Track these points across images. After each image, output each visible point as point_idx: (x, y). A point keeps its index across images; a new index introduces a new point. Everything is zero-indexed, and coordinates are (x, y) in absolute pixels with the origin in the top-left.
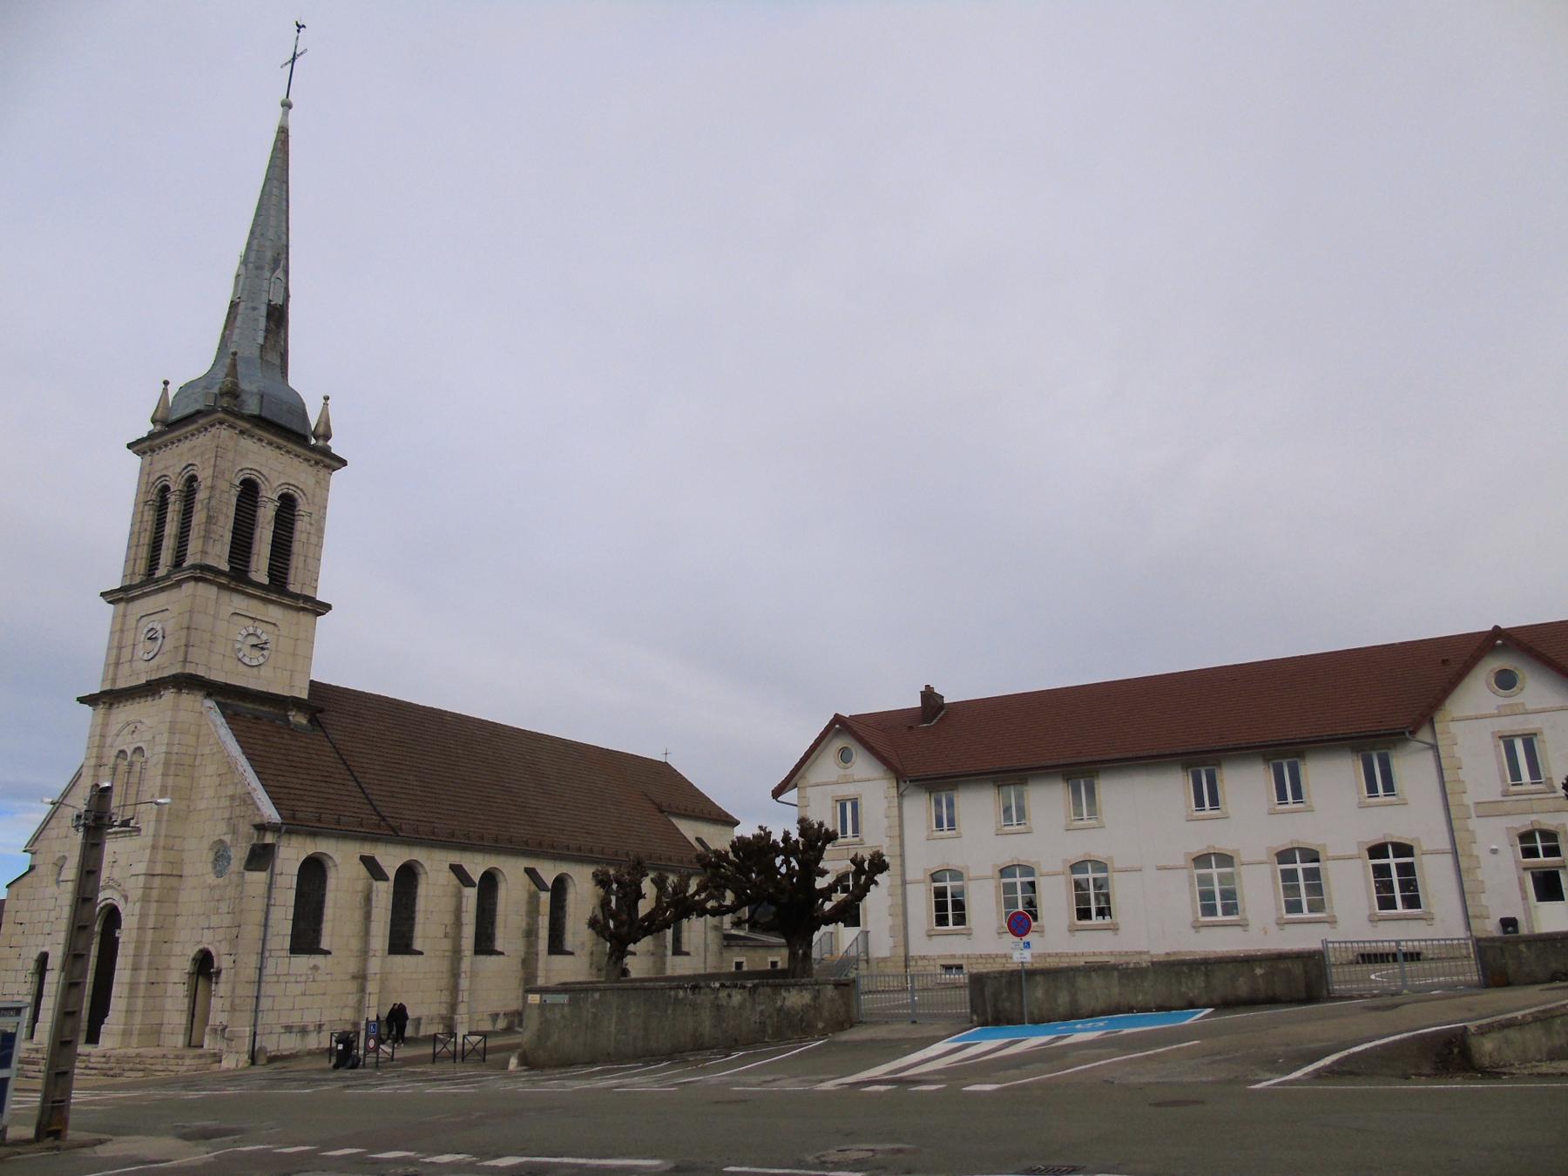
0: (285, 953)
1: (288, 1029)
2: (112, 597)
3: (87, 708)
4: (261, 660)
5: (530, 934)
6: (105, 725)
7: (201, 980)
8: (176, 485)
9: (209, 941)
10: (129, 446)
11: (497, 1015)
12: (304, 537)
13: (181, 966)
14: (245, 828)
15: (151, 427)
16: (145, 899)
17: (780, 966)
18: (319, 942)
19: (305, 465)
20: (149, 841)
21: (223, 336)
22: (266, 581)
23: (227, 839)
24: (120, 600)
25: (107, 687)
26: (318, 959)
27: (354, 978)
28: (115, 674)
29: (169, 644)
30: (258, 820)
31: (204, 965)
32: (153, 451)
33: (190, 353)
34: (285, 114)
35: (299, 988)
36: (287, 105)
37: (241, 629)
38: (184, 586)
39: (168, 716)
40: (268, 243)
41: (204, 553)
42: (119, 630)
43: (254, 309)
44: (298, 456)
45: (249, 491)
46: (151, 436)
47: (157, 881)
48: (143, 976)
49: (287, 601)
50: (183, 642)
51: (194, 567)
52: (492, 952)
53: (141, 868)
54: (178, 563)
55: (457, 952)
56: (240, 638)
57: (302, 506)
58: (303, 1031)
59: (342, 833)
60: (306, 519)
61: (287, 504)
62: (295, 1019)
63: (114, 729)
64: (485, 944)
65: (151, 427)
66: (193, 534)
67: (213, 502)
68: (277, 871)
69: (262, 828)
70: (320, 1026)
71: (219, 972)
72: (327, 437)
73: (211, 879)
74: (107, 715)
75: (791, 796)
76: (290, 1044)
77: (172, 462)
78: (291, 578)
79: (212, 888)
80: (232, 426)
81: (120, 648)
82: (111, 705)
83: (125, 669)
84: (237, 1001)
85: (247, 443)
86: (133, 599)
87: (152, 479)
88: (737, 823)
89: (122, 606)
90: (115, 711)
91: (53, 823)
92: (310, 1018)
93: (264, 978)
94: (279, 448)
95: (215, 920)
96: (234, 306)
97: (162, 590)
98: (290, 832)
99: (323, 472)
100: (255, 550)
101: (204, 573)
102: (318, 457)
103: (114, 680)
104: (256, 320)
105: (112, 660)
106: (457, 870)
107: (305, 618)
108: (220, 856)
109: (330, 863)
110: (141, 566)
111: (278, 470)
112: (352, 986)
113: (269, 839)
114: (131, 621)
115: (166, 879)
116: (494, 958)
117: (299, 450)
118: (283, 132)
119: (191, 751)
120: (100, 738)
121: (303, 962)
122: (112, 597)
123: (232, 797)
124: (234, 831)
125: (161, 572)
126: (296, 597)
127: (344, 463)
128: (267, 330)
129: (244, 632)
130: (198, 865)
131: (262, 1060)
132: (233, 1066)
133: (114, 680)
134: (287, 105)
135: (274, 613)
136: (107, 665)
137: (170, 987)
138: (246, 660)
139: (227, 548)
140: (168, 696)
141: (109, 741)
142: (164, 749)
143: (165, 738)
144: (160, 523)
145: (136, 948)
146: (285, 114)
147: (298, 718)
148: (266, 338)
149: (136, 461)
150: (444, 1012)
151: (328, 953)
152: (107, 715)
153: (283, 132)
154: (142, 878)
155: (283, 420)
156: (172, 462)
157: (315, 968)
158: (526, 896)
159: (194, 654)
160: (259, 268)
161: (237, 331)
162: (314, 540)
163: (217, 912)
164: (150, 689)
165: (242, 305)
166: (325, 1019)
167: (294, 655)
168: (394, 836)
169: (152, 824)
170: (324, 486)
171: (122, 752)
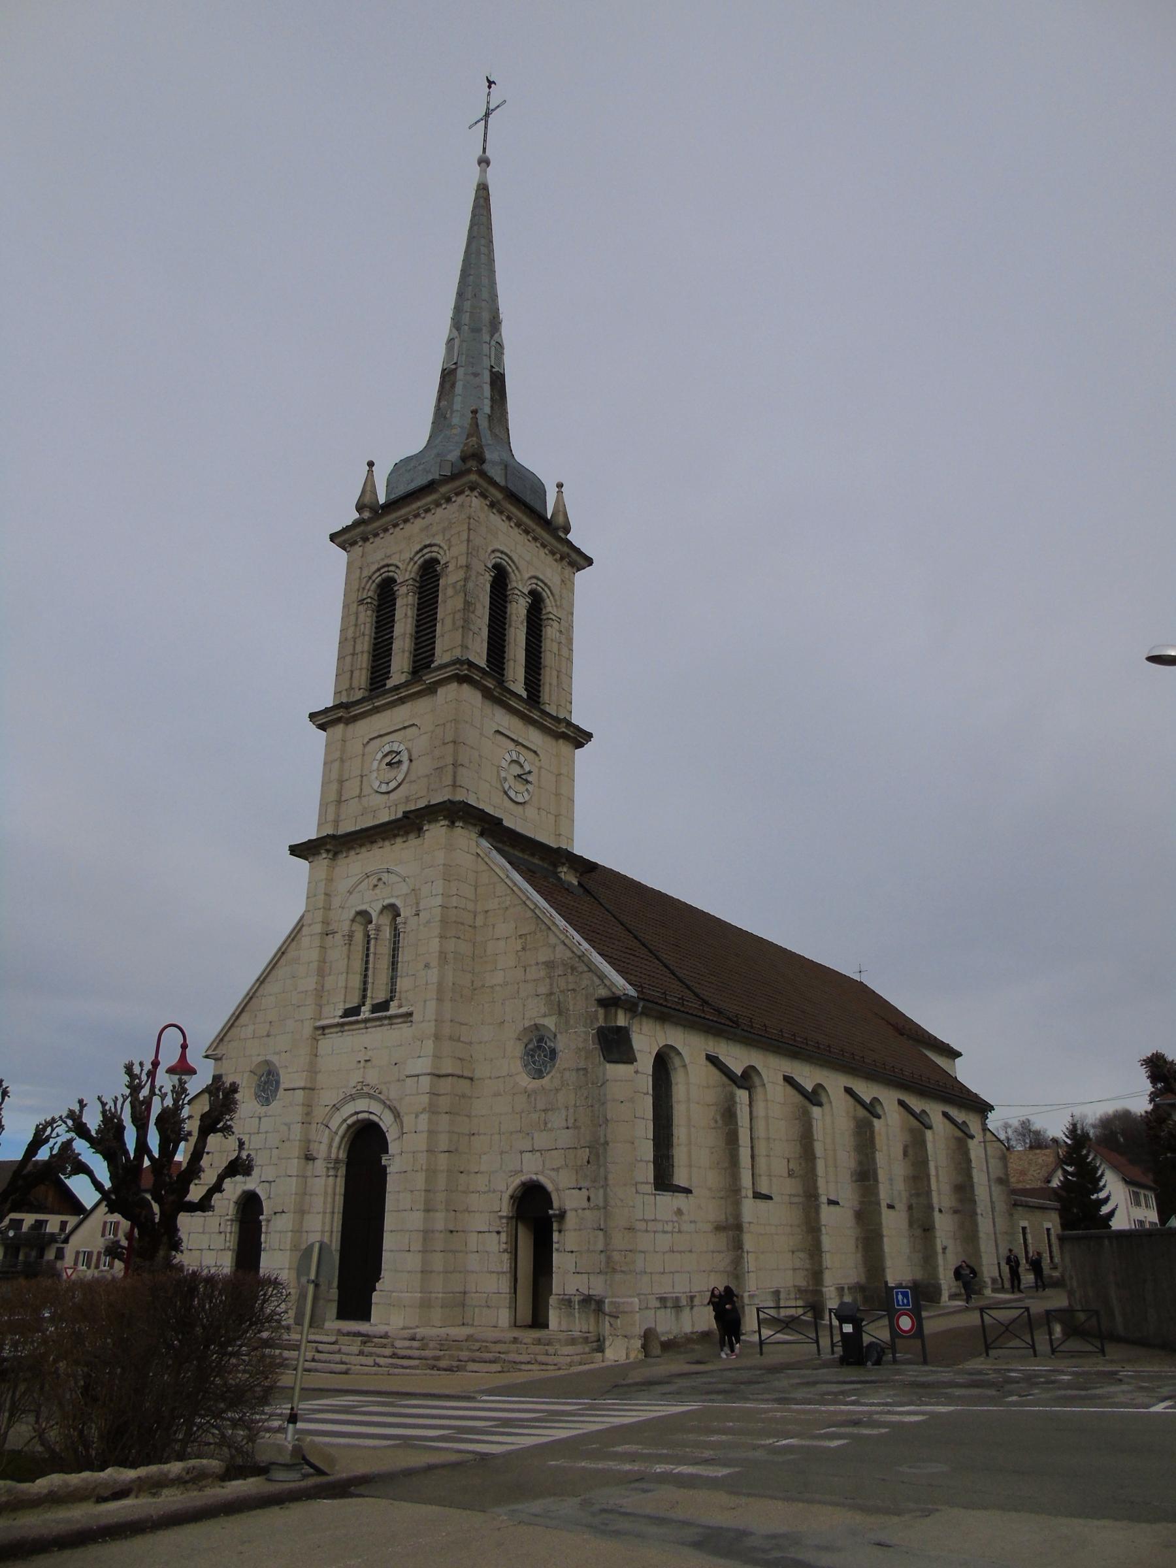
0: (650, 1188)
2: (323, 720)
3: (303, 864)
4: (527, 797)
6: (330, 880)
8: (406, 574)
9: (532, 1169)
10: (333, 537)
11: (843, 1288)
12: (555, 647)
13: (490, 1203)
14: (579, 1005)
15: (357, 515)
16: (432, 1110)
18: (671, 1175)
19: (550, 559)
20: (430, 1028)
21: (438, 408)
23: (550, 1022)
24: (338, 720)
25: (329, 830)
27: (719, 1228)
28: (338, 815)
29: (423, 766)
30: (603, 992)
31: (533, 1211)
32: (365, 539)
33: (401, 427)
34: (483, 172)
35: (664, 1241)
37: (505, 753)
38: (441, 691)
39: (440, 857)
40: (484, 304)
41: (464, 647)
42: (336, 762)
44: (544, 546)
46: (356, 524)
47: (445, 1085)
48: (440, 1220)
50: (450, 760)
53: (423, 1065)
56: (504, 764)
57: (550, 606)
60: (555, 624)
61: (536, 602)
62: (664, 1287)
63: (343, 886)
65: (357, 515)
66: (485, 599)
67: (470, 585)
69: (610, 1003)
70: (692, 1298)
71: (562, 1216)
72: (567, 530)
73: (525, 1081)
74: (331, 868)
77: (400, 550)
79: (528, 1094)
80: (483, 495)
81: (341, 782)
82: (336, 854)
83: (352, 808)
84: (616, 1256)
85: (495, 519)
86: (355, 719)
87: (366, 573)
89: (339, 729)
90: (342, 861)
91: (244, 1018)
92: (680, 1287)
94: (527, 532)
95: (541, 1140)
96: (448, 377)
97: (402, 701)
98: (646, 1014)
99: (568, 570)
101: (464, 673)
103: (336, 822)
104: (480, 387)
105: (333, 796)
107: (564, 747)
108: (539, 1051)
109: (677, 1062)
110: (362, 678)
112: (721, 1241)
113: (621, 1020)
114: (355, 747)
115: (455, 1082)
118: (483, 192)
119: (470, 906)
120: (321, 898)
122: (323, 720)
123: (550, 965)
124: (560, 1011)
127: (589, 561)
128: (492, 399)
129: (509, 759)
130: (503, 1062)
131: (656, 1350)
132: (622, 1359)
133: (336, 822)
134: (484, 162)
135: (534, 737)
136: (324, 805)
137: (473, 1239)
138: (512, 794)
139: (485, 645)
140: (436, 832)
141: (336, 902)
142: (439, 901)
143: (439, 887)
145: (428, 1180)
146: (483, 172)
148: (492, 407)
149: (339, 557)
150: (802, 1283)
151: (688, 1191)
152: (331, 868)
153: (483, 192)
154: (425, 1081)
155: (529, 498)
156: (400, 550)
157: (679, 1212)
158: (852, 1125)
159: (466, 777)
160: (476, 330)
161: (458, 399)
162: (565, 652)
163: (544, 1126)
164: (409, 824)
165: (460, 372)
166: (695, 1289)
167: (558, 795)
169: (432, 1005)
170: (568, 584)
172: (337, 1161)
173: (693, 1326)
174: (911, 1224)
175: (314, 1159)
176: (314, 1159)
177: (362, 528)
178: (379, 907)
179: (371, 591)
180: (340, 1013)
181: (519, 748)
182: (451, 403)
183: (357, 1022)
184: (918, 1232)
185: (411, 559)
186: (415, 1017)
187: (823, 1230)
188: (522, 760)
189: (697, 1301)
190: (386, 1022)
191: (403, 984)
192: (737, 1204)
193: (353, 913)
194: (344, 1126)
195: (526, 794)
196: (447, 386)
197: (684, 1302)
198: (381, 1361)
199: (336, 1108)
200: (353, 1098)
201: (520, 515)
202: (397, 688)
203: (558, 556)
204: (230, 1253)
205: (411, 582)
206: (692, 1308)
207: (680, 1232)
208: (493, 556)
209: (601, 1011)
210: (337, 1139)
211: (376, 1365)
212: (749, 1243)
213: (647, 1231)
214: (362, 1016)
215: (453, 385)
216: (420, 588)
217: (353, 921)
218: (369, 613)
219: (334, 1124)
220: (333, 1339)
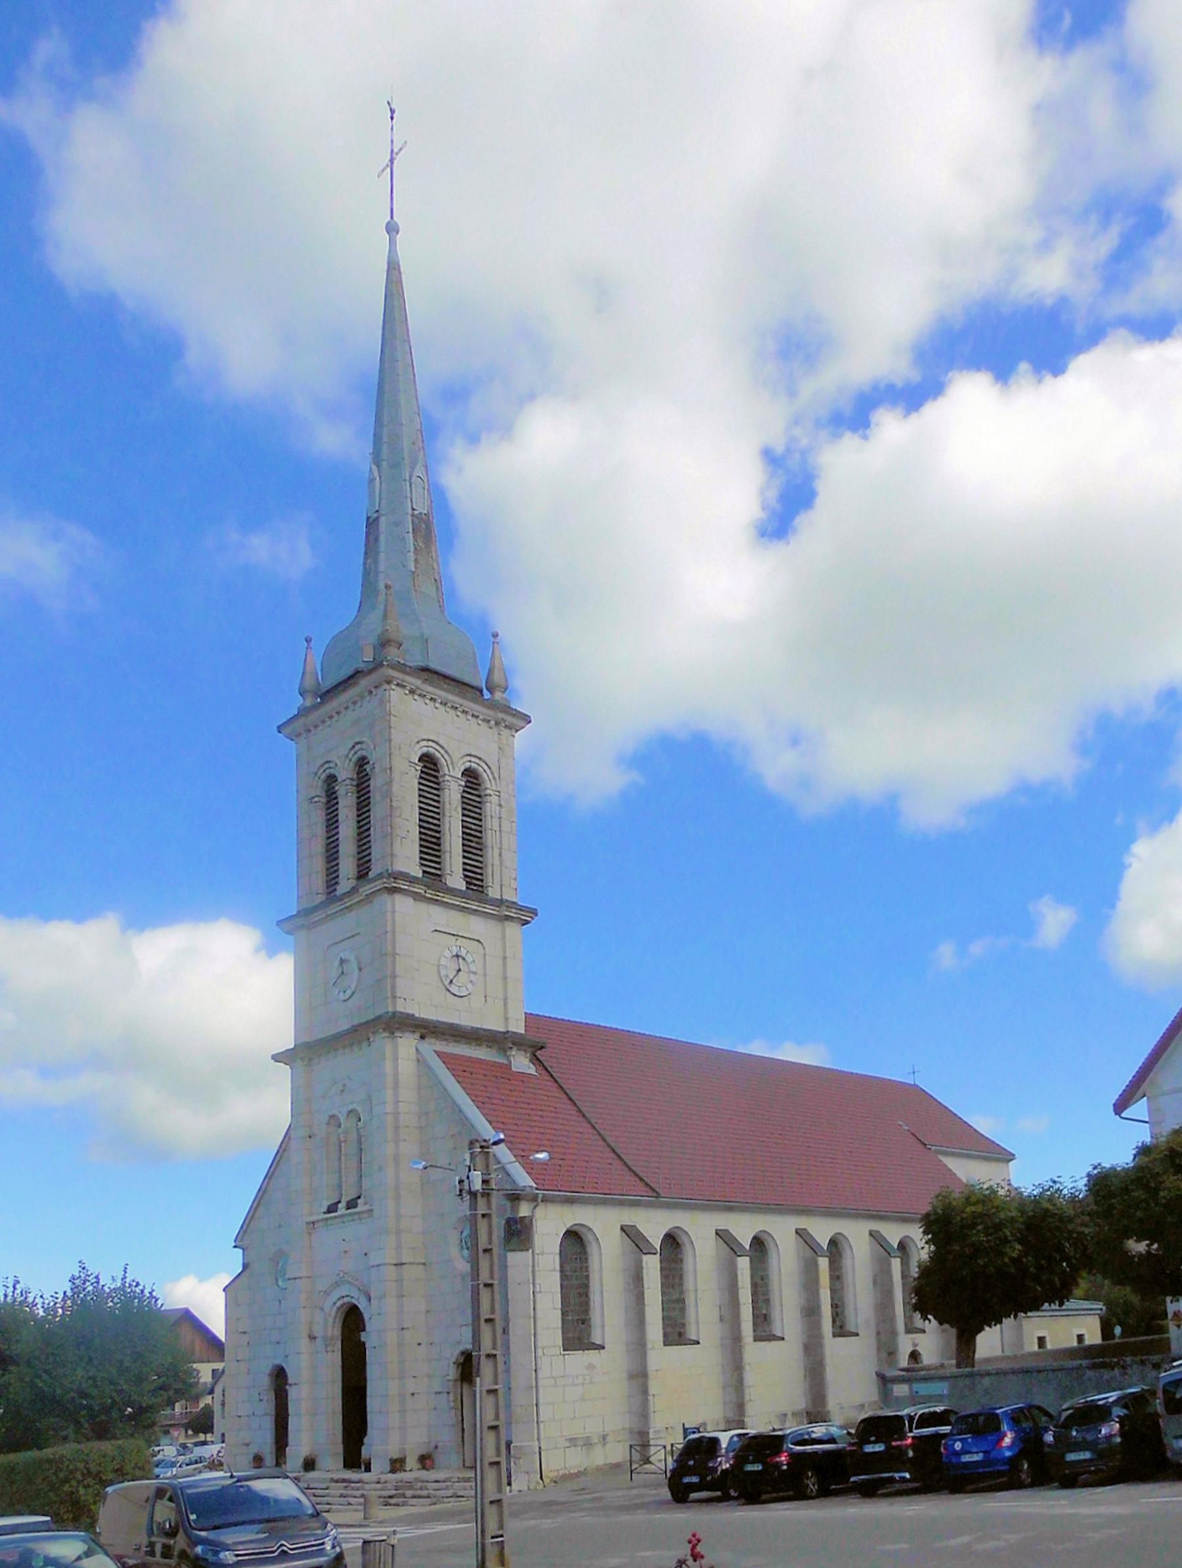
1: (573, 1442)
5: (811, 1312)
7: (465, 1387)
8: (345, 772)
11: (785, 1415)
17: (1088, 1341)
22: (462, 886)
26: (591, 1356)
36: (392, 229)
43: (397, 524)
45: (430, 765)
46: (303, 712)
49: (489, 909)
51: (380, 876)
52: (772, 1338)
54: (363, 874)
55: (736, 1340)
58: (588, 1444)
59: (607, 1199)
61: (471, 776)
64: (764, 1330)
68: (537, 1251)
70: (604, 1437)
75: (1140, 1108)
76: (576, 1460)
78: (489, 881)
88: (1008, 1157)
92: (593, 1429)
93: (541, 1382)
99: (506, 732)
100: (446, 846)
102: (501, 715)
106: (723, 1235)
111: (458, 736)
116: (774, 1344)
117: (476, 708)
121: (580, 1359)
125: (344, 886)
126: (500, 903)
135: (477, 926)
140: (381, 1041)
144: (332, 823)
146: (392, 243)
147: (521, 1063)
150: (730, 1415)
157: (591, 1367)
168: (653, 1195)
171: (332, 1117)
172: (332, 1338)
173: (606, 1457)
174: (879, 1349)
175: (315, 1338)
176: (315, 1338)
177: (302, 721)
178: (344, 1111)
179: (319, 789)
180: (325, 1209)
181: (460, 941)
182: (376, 562)
183: (335, 1217)
184: (885, 1355)
185: (347, 756)
186: (376, 1213)
187: (747, 1367)
188: (463, 953)
189: (609, 1439)
190: (356, 1217)
191: (366, 1184)
192: (643, 1355)
193: (327, 1118)
194: (335, 1309)
195: (470, 986)
196: (372, 538)
197: (595, 1440)
198: (352, 1500)
199: (327, 1293)
200: (337, 1284)
201: (443, 694)
202: (348, 894)
203: (493, 723)
204: (268, 1418)
205: (348, 782)
206: (604, 1444)
207: (591, 1383)
208: (418, 746)
209: (509, 1204)
210: (331, 1320)
211: (349, 1504)
212: (653, 1388)
213: (555, 1386)
214: (339, 1213)
215: (377, 540)
216: (358, 786)
217: (328, 1124)
218: (319, 812)
219: (327, 1308)
220: (324, 1486)
